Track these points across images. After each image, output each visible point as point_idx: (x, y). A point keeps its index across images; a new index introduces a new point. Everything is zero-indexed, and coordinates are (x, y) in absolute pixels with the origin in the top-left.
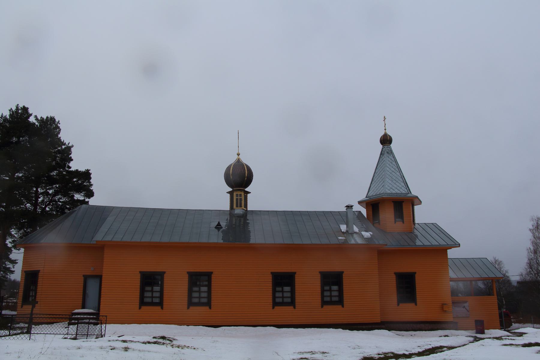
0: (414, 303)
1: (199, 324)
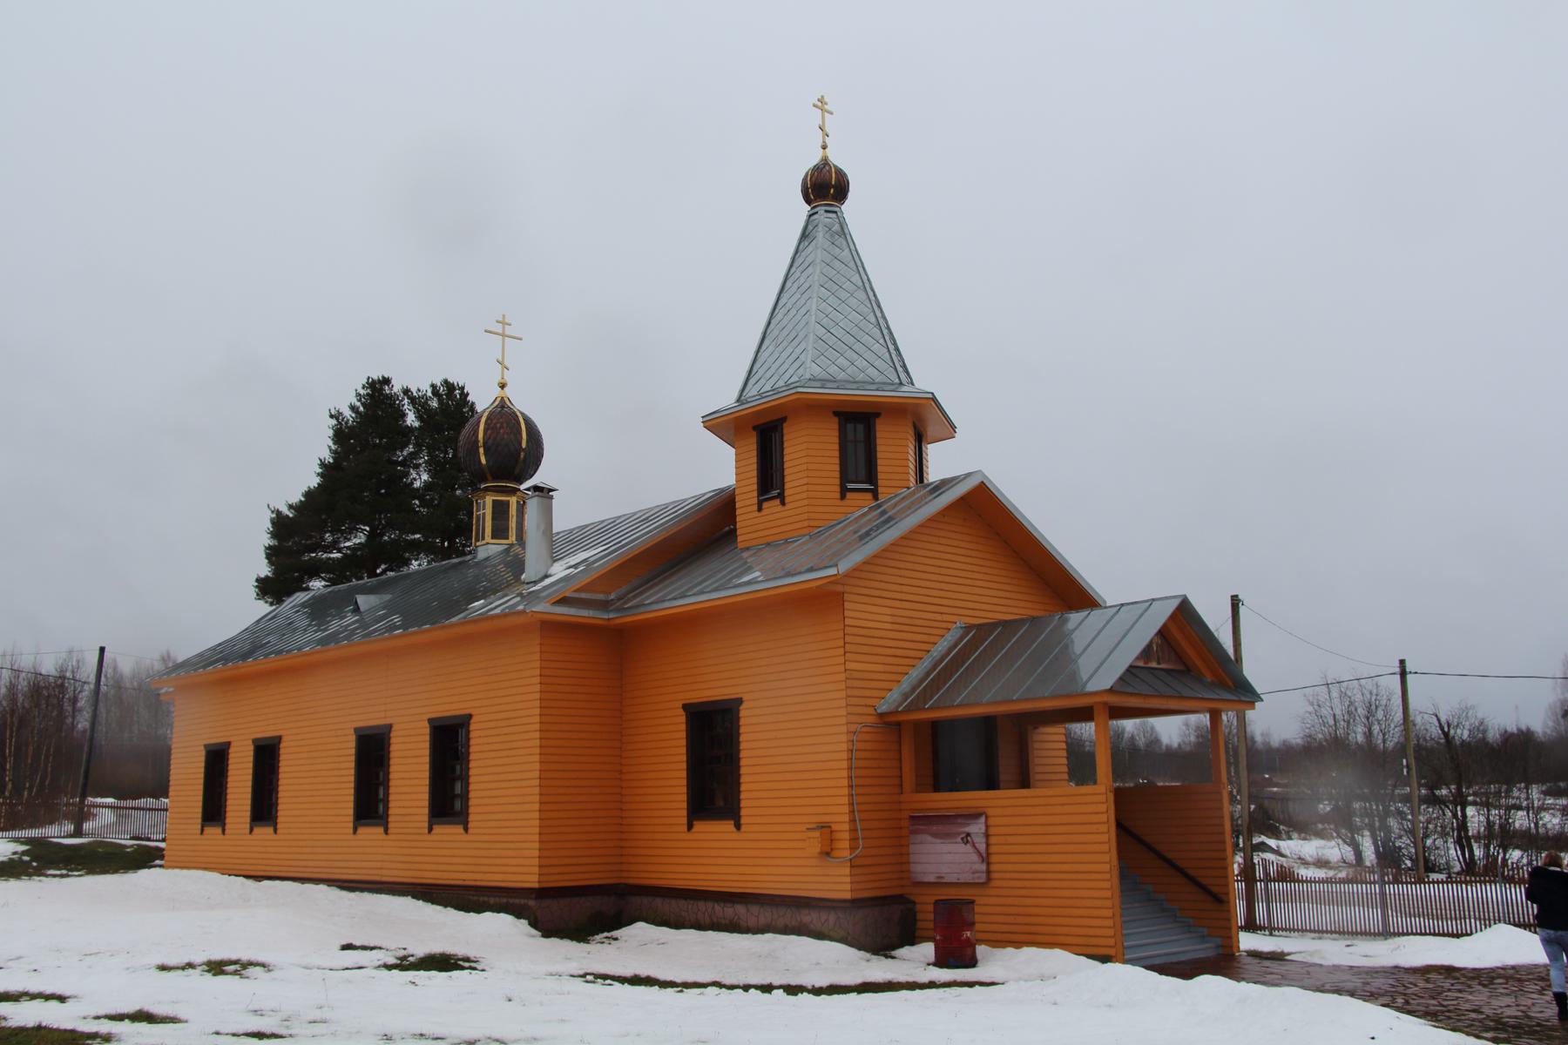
0: (732, 822)
1: (174, 864)
